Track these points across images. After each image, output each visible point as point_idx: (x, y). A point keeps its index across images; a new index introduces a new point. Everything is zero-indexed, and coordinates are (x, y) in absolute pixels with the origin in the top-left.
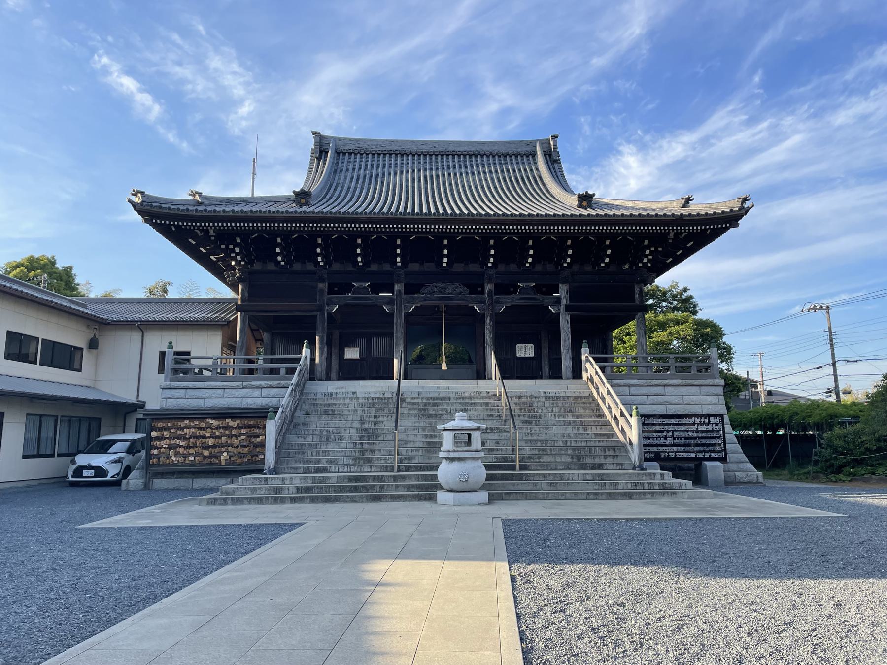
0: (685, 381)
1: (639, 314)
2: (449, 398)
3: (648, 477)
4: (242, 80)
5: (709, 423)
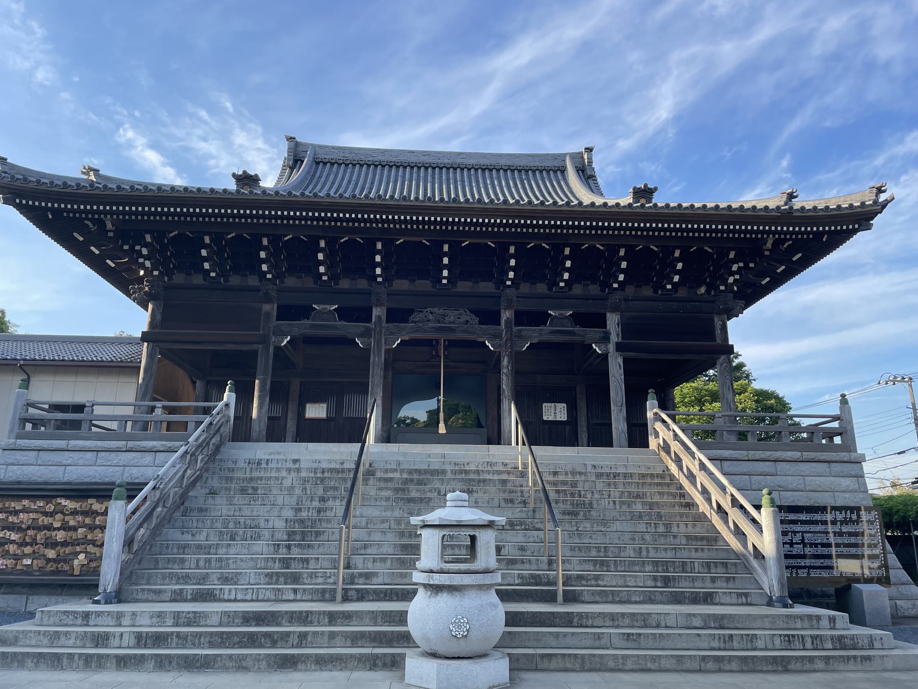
1: (723, 357)
2: (444, 472)
3: (806, 624)
4: (266, 156)
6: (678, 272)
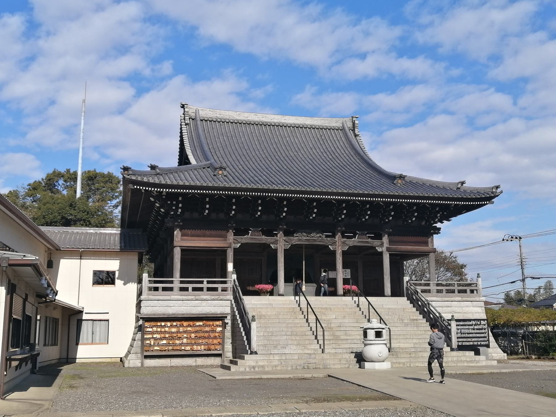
0: (465, 299)
5: (480, 324)
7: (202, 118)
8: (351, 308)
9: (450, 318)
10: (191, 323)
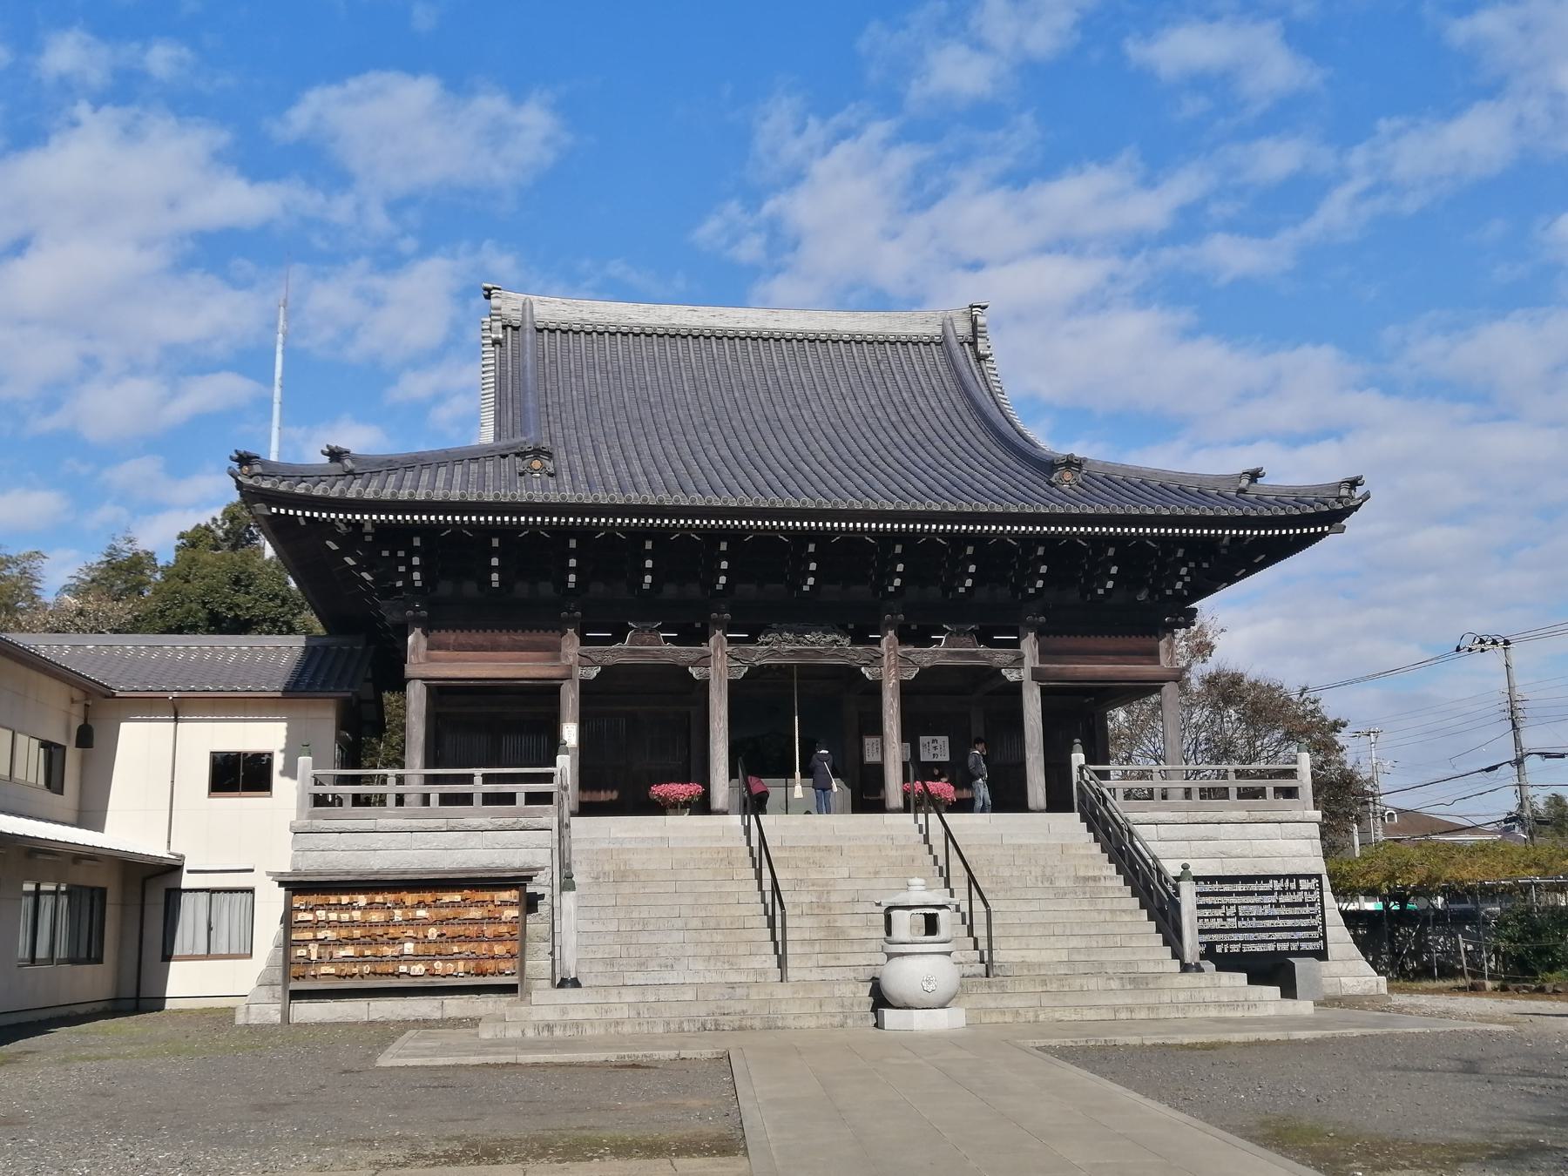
6: (971, 575)
7: (540, 325)
8: (904, 847)
9: (1178, 871)
10: (428, 897)
